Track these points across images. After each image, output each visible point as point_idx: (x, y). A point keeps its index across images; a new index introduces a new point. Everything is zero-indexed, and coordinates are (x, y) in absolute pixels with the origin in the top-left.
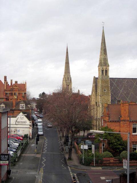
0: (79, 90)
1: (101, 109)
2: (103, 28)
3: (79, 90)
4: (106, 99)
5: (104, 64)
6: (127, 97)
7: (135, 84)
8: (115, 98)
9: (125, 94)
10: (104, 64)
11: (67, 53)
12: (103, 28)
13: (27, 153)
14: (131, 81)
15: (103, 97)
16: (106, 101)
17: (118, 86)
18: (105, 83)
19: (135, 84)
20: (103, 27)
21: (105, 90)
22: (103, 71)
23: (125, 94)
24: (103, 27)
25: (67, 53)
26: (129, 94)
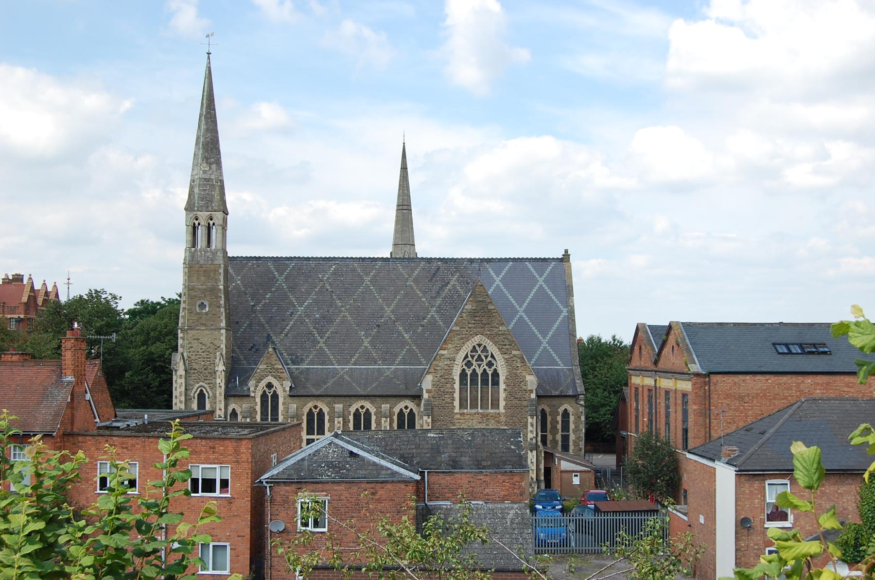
0: (566, 251)
1: (183, 380)
2: (209, 58)
3: (566, 251)
4: (205, 340)
5: (208, 200)
6: (321, 334)
7: (367, 279)
8: (269, 337)
9: (316, 322)
10: (208, 200)
11: (404, 168)
12: (209, 58)
13: (60, 473)
14: (354, 270)
15: (194, 332)
16: (203, 347)
17: (292, 289)
18: (203, 278)
19: (367, 279)
20: (209, 54)
21: (202, 306)
22: (195, 228)
23: (316, 322)
24: (209, 54)
25: (404, 168)
26: (330, 321)
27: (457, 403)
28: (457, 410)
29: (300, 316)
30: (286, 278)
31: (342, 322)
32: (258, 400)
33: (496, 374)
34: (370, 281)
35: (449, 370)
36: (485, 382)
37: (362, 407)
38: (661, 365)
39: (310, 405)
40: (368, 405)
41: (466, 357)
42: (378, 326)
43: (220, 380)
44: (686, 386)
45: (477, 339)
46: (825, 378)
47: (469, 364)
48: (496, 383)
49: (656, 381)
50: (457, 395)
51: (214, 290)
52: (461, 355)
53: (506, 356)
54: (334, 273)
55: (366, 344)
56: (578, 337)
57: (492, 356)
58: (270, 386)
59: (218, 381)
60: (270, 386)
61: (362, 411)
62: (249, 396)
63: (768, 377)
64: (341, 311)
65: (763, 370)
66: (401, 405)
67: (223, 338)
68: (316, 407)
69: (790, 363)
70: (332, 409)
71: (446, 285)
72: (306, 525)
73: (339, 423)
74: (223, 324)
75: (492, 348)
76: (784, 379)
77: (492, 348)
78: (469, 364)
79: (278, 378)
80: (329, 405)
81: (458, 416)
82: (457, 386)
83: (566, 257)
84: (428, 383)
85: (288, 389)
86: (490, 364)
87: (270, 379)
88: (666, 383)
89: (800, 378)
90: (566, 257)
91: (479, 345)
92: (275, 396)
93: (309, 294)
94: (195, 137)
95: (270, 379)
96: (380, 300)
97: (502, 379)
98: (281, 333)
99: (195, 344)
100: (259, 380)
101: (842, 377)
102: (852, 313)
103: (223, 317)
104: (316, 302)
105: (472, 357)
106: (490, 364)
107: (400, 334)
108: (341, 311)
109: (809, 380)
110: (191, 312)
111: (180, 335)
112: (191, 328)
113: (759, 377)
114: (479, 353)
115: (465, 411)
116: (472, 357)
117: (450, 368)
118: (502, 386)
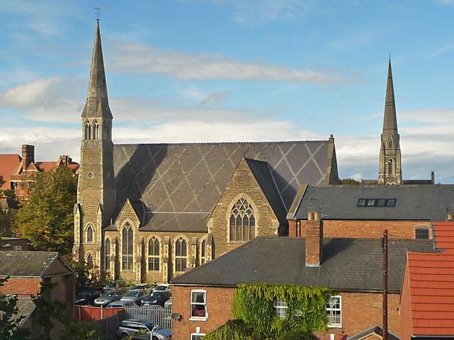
0: (332, 136)
3: (332, 136)
4: (92, 196)
25: (390, 77)
27: (228, 237)
28: (228, 242)
29: (160, 181)
31: (183, 184)
32: (121, 233)
33: (252, 218)
35: (224, 216)
36: (246, 223)
37: (181, 238)
39: (151, 236)
40: (184, 237)
41: (234, 207)
42: (205, 187)
43: (99, 221)
45: (241, 195)
47: (236, 212)
50: (228, 232)
51: (97, 166)
52: (231, 205)
53: (259, 206)
54: (185, 153)
55: (195, 198)
57: (250, 206)
58: (127, 224)
59: (98, 221)
60: (127, 224)
61: (154, 240)
62: (117, 230)
63: (339, 221)
64: (184, 178)
65: (337, 217)
66: (177, 237)
67: (102, 195)
68: (154, 237)
69: (366, 212)
70: (163, 239)
72: (338, 313)
73: (166, 248)
74: (102, 186)
76: (350, 223)
77: (250, 201)
78: (236, 212)
79: (133, 220)
80: (162, 236)
81: (228, 245)
82: (228, 225)
83: (332, 138)
84: (210, 224)
85: (138, 226)
86: (249, 212)
87: (128, 220)
89: (361, 223)
90: (332, 138)
91: (242, 199)
92: (131, 230)
93: (168, 167)
95: (128, 220)
96: (209, 170)
99: (87, 198)
100: (122, 221)
101: (391, 222)
103: (102, 182)
104: (171, 171)
107: (216, 191)
108: (184, 178)
109: (368, 224)
110: (84, 178)
111: (78, 193)
112: (84, 188)
114: (241, 204)
115: (234, 242)
116: (238, 207)
117: (224, 214)
118: (257, 226)
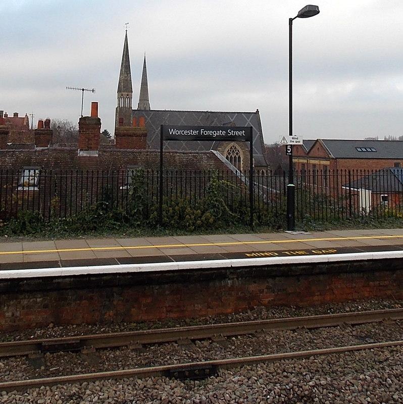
0: (257, 110)
3: (257, 110)
20: (126, 31)
24: (126, 31)
30: (150, 119)
33: (239, 157)
34: (250, 121)
36: (235, 161)
38: (310, 155)
41: (228, 151)
44: (328, 163)
46: (376, 161)
48: (239, 161)
49: (307, 161)
56: (102, 131)
57: (238, 151)
71: (213, 122)
75: (238, 148)
77: (238, 148)
78: (229, 154)
83: (258, 111)
86: (237, 154)
88: (312, 162)
90: (258, 111)
91: (233, 146)
94: (310, 18)
97: (242, 159)
98: (151, 140)
102: (40, 122)
105: (231, 151)
106: (237, 154)
109: (371, 161)
113: (353, 160)
